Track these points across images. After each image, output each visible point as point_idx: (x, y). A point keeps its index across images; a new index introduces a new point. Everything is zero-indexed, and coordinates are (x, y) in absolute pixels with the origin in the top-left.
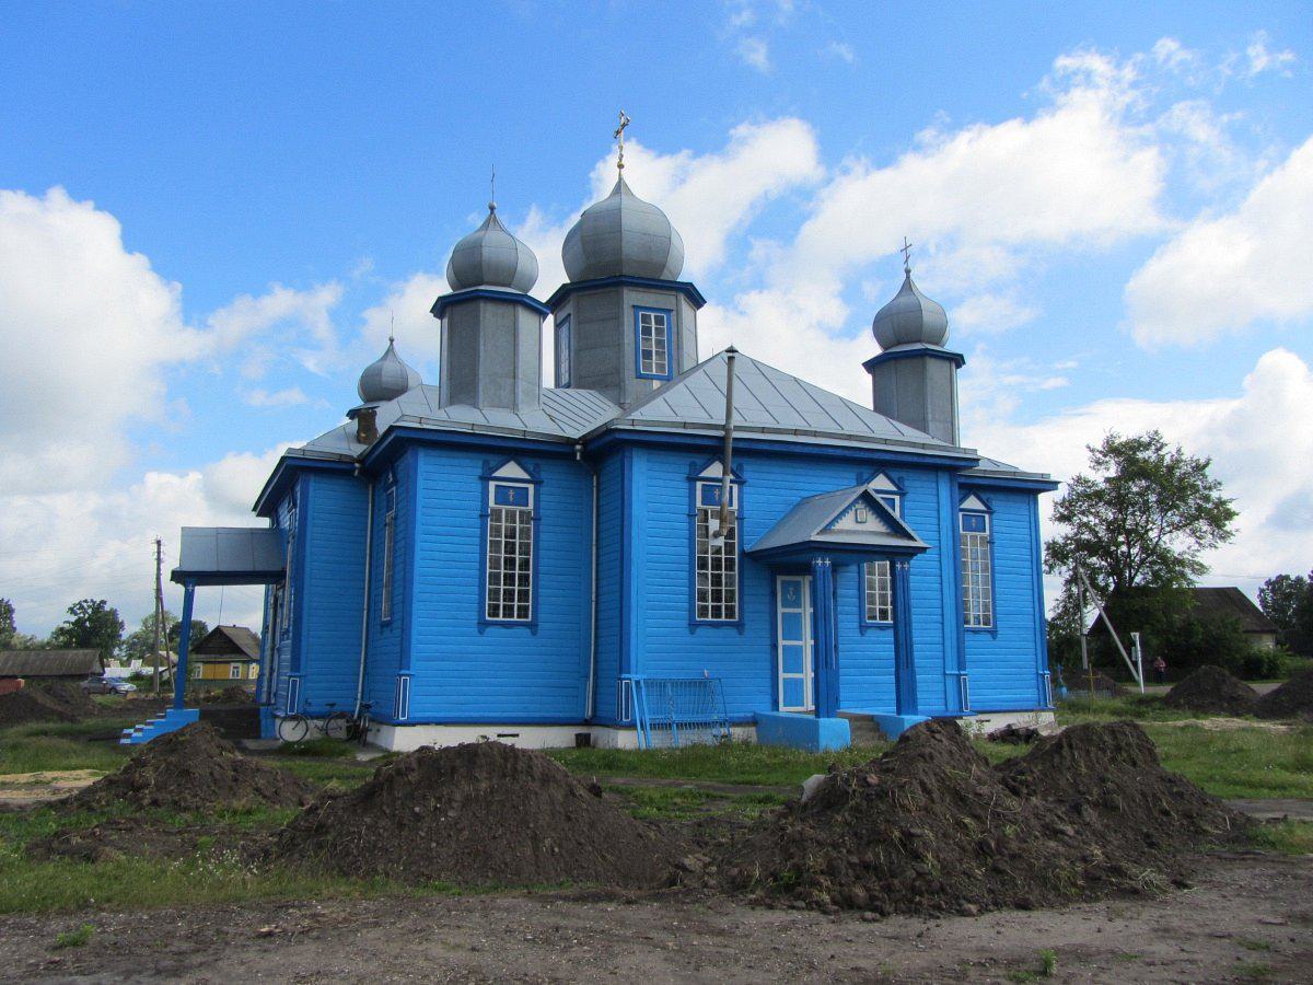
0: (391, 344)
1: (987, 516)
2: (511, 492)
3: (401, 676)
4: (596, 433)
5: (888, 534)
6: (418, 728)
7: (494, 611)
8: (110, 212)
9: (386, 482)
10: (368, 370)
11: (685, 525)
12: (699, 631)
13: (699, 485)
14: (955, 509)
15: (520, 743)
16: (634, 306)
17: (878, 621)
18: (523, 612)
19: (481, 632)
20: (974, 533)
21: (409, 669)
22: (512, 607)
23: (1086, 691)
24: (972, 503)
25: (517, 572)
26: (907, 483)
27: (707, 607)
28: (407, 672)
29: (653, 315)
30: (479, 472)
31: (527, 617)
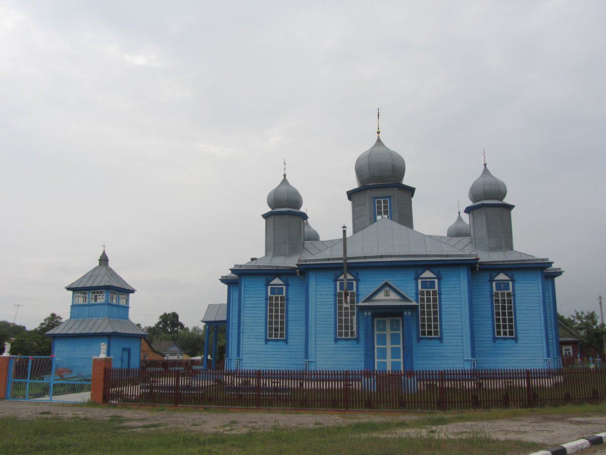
0: (485, 167)
1: (510, 283)
2: (277, 290)
5: (400, 300)
7: (271, 335)
10: (472, 188)
11: (333, 300)
12: (339, 342)
17: (427, 336)
18: (436, 333)
19: (494, 342)
20: (503, 291)
22: (506, 325)
23: (113, 363)
26: (441, 273)
27: (342, 332)
30: (265, 283)
31: (438, 335)
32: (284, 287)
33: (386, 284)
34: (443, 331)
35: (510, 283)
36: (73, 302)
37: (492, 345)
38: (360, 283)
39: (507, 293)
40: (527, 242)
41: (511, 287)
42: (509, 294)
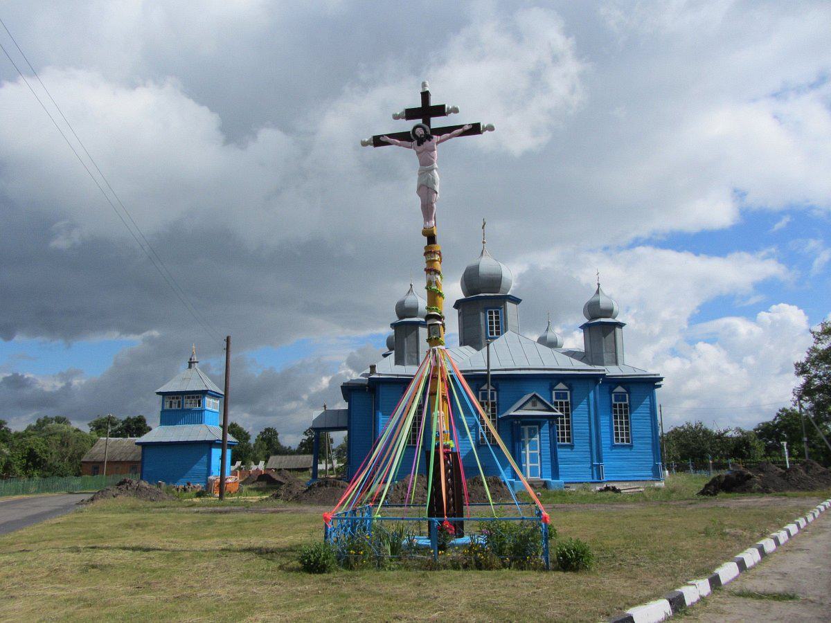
32: (568, 392)
33: (535, 396)
34: (651, 442)
35: (627, 395)
36: (163, 407)
37: (609, 451)
38: (500, 393)
39: (625, 404)
40: (634, 359)
41: (627, 399)
42: (567, 403)
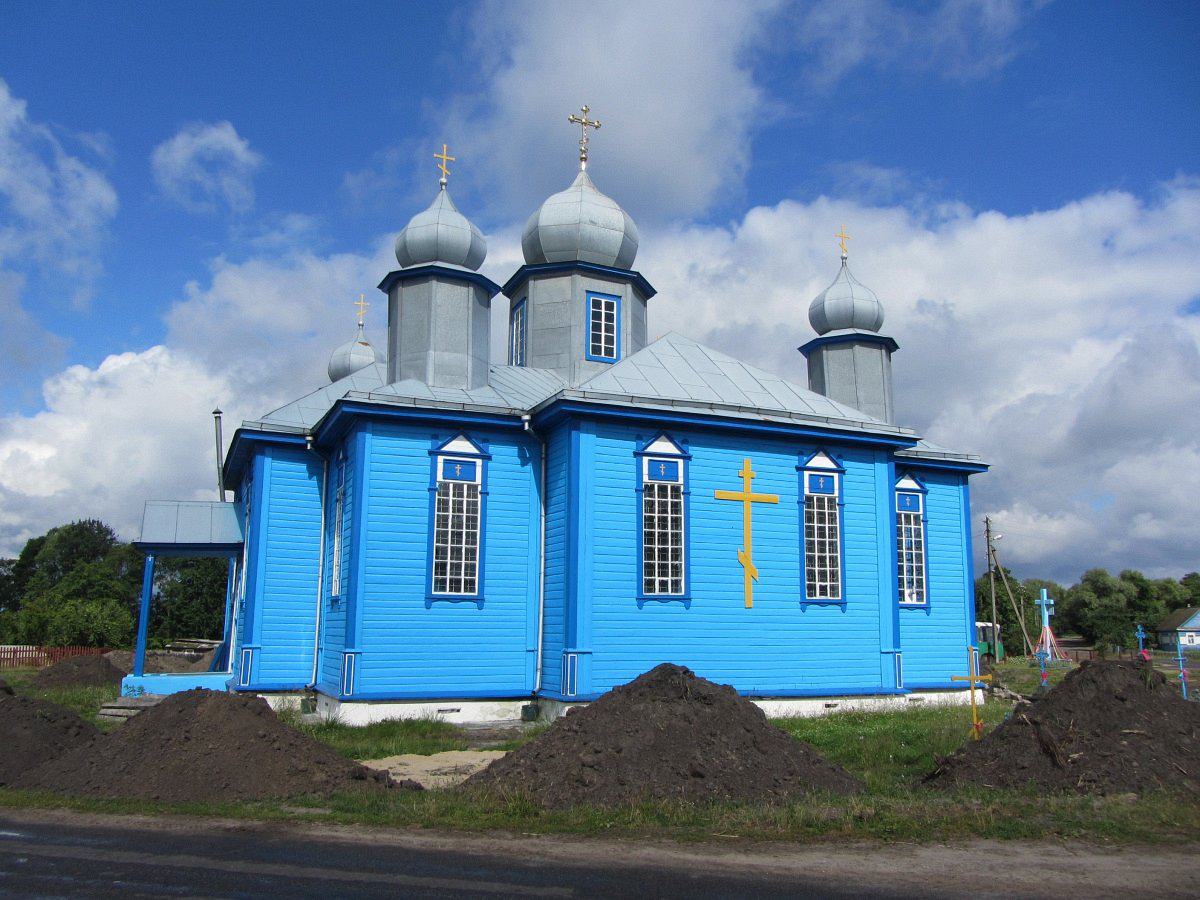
3: (568, 653)
4: (543, 407)
6: (362, 706)
8: (413, 215)
9: (338, 458)
13: (646, 460)
14: (893, 489)
15: (453, 719)
16: (587, 291)
21: (353, 648)
24: (907, 483)
25: (464, 546)
28: (250, 646)
29: (603, 301)
